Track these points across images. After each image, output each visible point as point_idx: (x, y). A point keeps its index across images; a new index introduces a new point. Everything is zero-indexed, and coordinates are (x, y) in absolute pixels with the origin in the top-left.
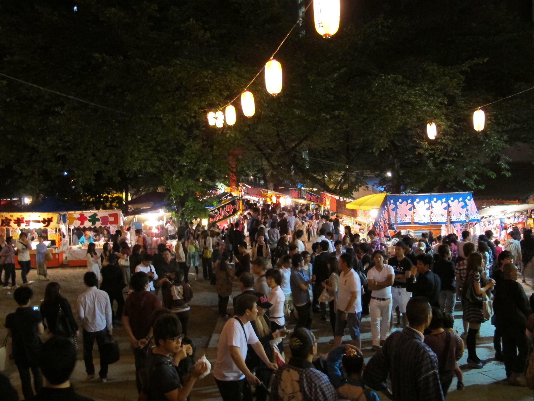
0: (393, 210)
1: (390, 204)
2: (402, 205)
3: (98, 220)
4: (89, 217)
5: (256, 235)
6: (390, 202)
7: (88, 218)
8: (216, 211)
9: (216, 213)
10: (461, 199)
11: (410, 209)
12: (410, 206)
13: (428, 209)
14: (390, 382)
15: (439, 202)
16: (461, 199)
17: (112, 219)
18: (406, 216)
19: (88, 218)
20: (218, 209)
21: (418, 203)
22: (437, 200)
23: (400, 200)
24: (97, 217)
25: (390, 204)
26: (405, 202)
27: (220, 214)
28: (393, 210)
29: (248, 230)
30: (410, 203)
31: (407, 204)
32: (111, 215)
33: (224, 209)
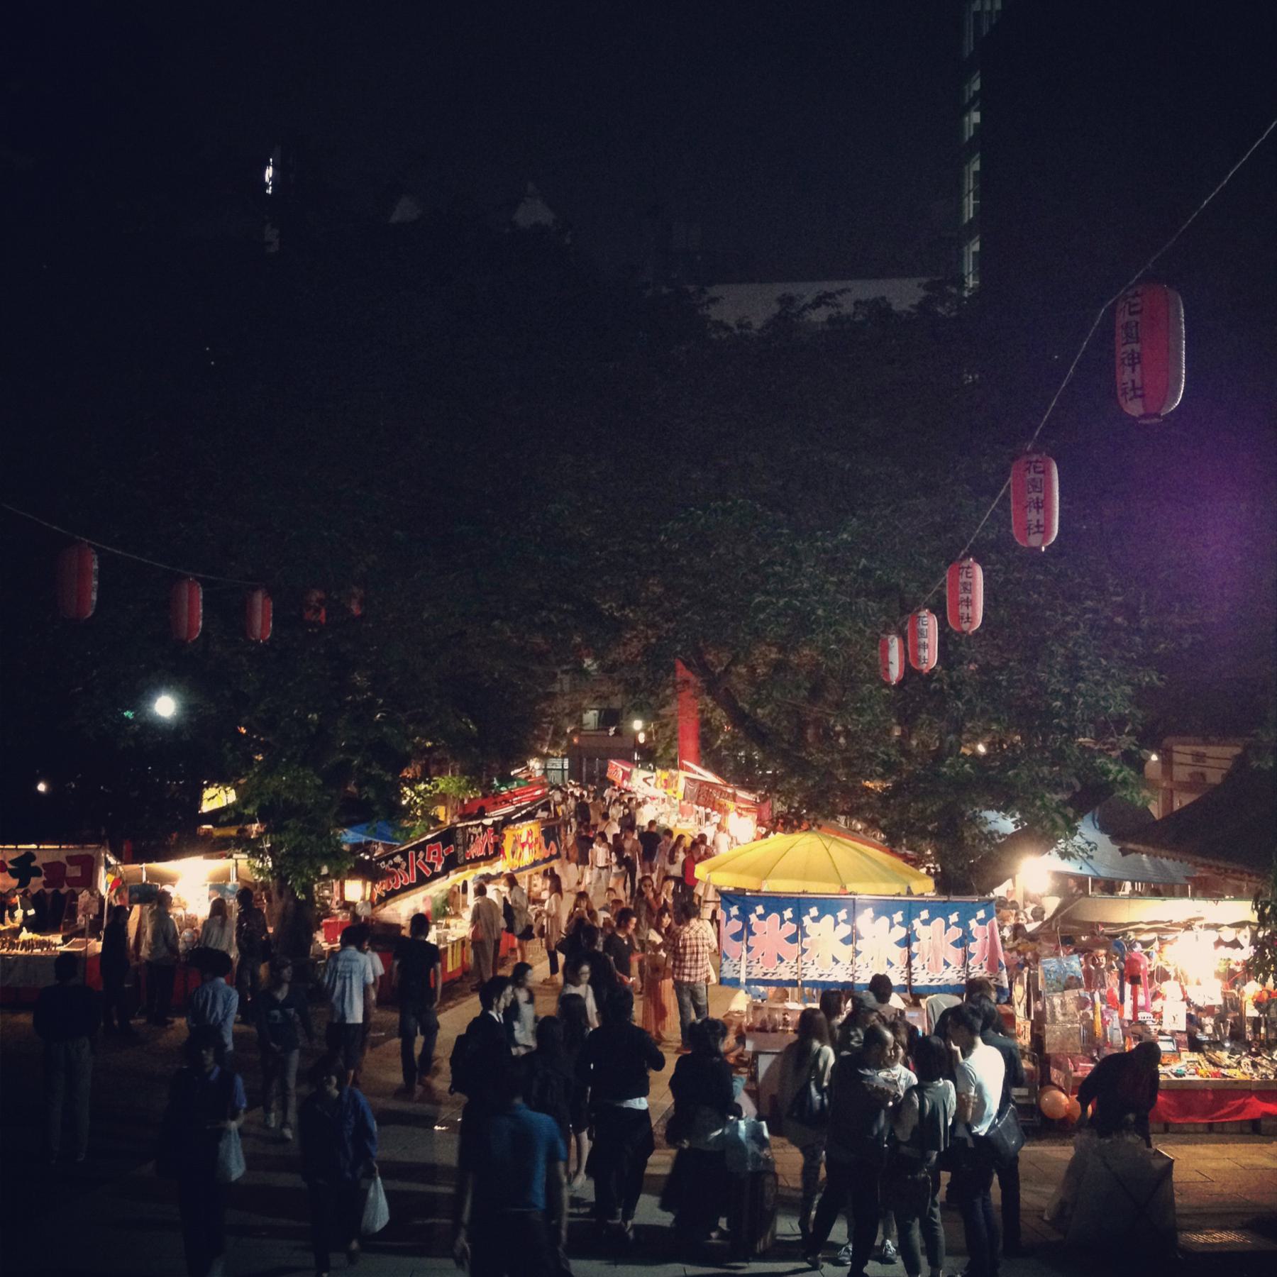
0: (737, 937)
1: (729, 918)
2: (766, 923)
3: (37, 872)
4: (12, 862)
5: (826, 1101)
6: (728, 913)
7: (10, 866)
8: (398, 859)
9: (397, 866)
10: (954, 918)
11: (793, 939)
12: (790, 928)
13: (793, 939)
14: (230, 801)
15: (939, 922)
16: (954, 918)
17: (74, 872)
18: (781, 960)
19: (10, 866)
20: (404, 855)
21: (815, 920)
22: (989, 916)
23: (760, 910)
24: (33, 864)
25: (729, 918)
26: (774, 917)
27: (407, 870)
28: (737, 937)
29: (956, 1052)
30: (844, 921)
31: (783, 922)
32: (72, 860)
33: (421, 854)
